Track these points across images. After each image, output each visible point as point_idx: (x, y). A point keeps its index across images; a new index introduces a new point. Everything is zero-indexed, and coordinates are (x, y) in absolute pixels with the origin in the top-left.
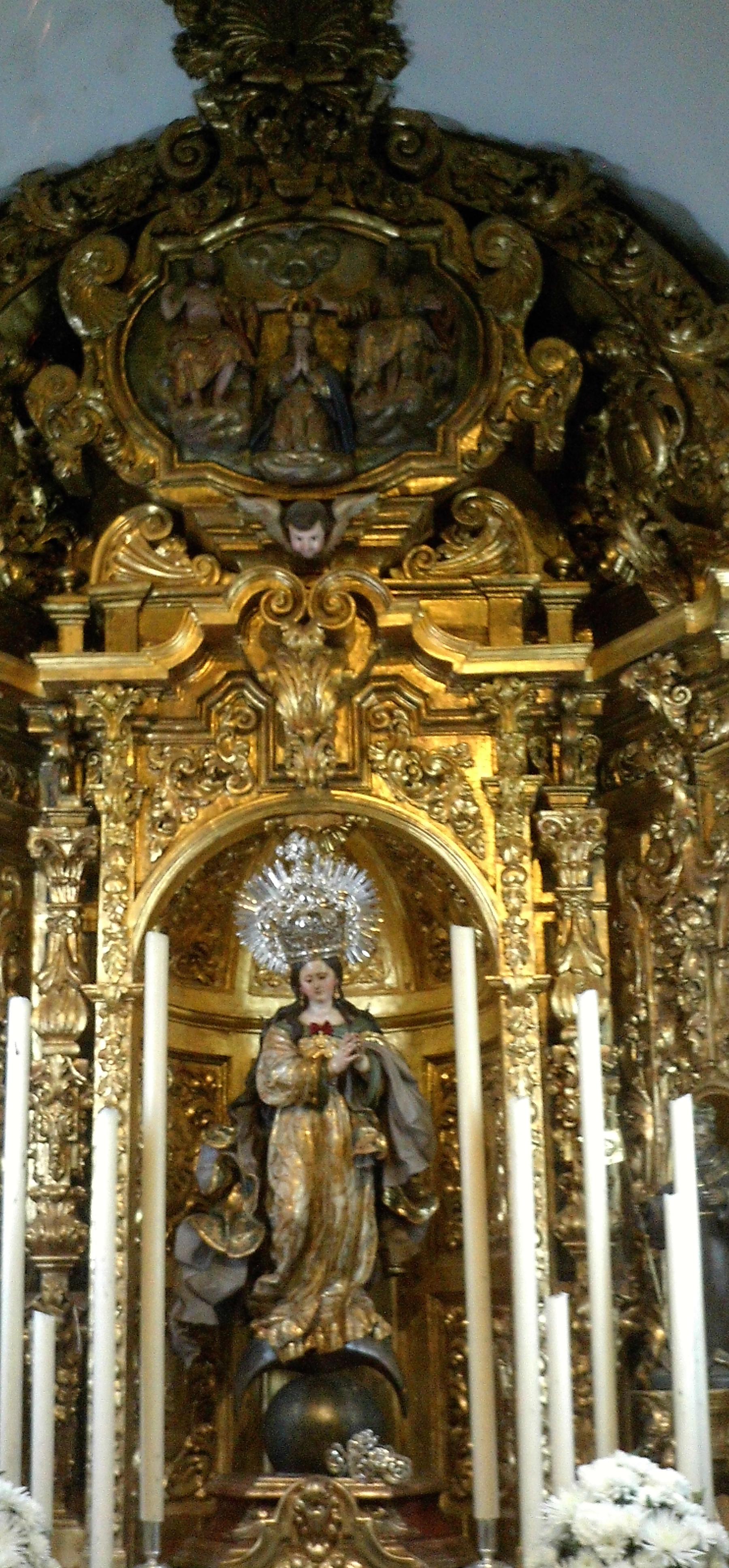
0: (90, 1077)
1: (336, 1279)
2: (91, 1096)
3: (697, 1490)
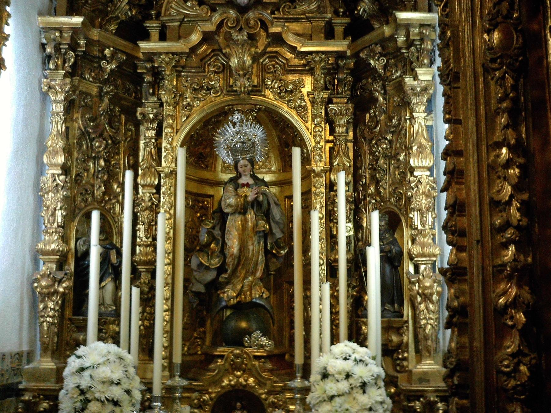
0: (159, 201)
1: (249, 276)
2: (160, 208)
3: (374, 355)
